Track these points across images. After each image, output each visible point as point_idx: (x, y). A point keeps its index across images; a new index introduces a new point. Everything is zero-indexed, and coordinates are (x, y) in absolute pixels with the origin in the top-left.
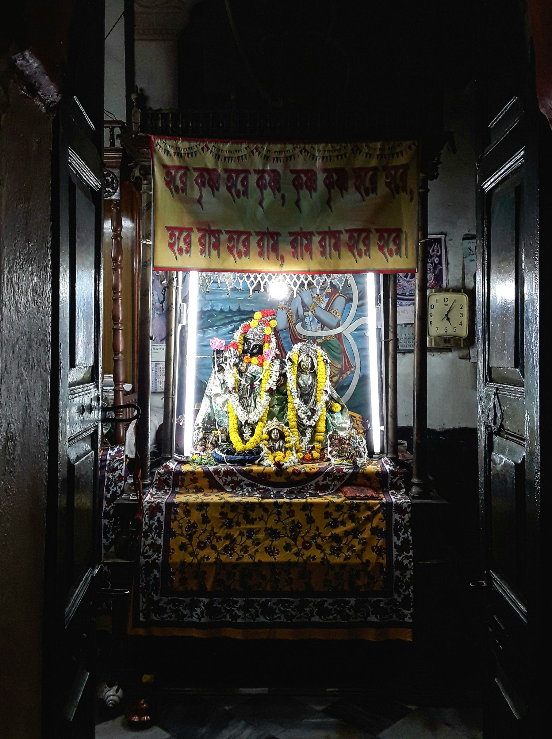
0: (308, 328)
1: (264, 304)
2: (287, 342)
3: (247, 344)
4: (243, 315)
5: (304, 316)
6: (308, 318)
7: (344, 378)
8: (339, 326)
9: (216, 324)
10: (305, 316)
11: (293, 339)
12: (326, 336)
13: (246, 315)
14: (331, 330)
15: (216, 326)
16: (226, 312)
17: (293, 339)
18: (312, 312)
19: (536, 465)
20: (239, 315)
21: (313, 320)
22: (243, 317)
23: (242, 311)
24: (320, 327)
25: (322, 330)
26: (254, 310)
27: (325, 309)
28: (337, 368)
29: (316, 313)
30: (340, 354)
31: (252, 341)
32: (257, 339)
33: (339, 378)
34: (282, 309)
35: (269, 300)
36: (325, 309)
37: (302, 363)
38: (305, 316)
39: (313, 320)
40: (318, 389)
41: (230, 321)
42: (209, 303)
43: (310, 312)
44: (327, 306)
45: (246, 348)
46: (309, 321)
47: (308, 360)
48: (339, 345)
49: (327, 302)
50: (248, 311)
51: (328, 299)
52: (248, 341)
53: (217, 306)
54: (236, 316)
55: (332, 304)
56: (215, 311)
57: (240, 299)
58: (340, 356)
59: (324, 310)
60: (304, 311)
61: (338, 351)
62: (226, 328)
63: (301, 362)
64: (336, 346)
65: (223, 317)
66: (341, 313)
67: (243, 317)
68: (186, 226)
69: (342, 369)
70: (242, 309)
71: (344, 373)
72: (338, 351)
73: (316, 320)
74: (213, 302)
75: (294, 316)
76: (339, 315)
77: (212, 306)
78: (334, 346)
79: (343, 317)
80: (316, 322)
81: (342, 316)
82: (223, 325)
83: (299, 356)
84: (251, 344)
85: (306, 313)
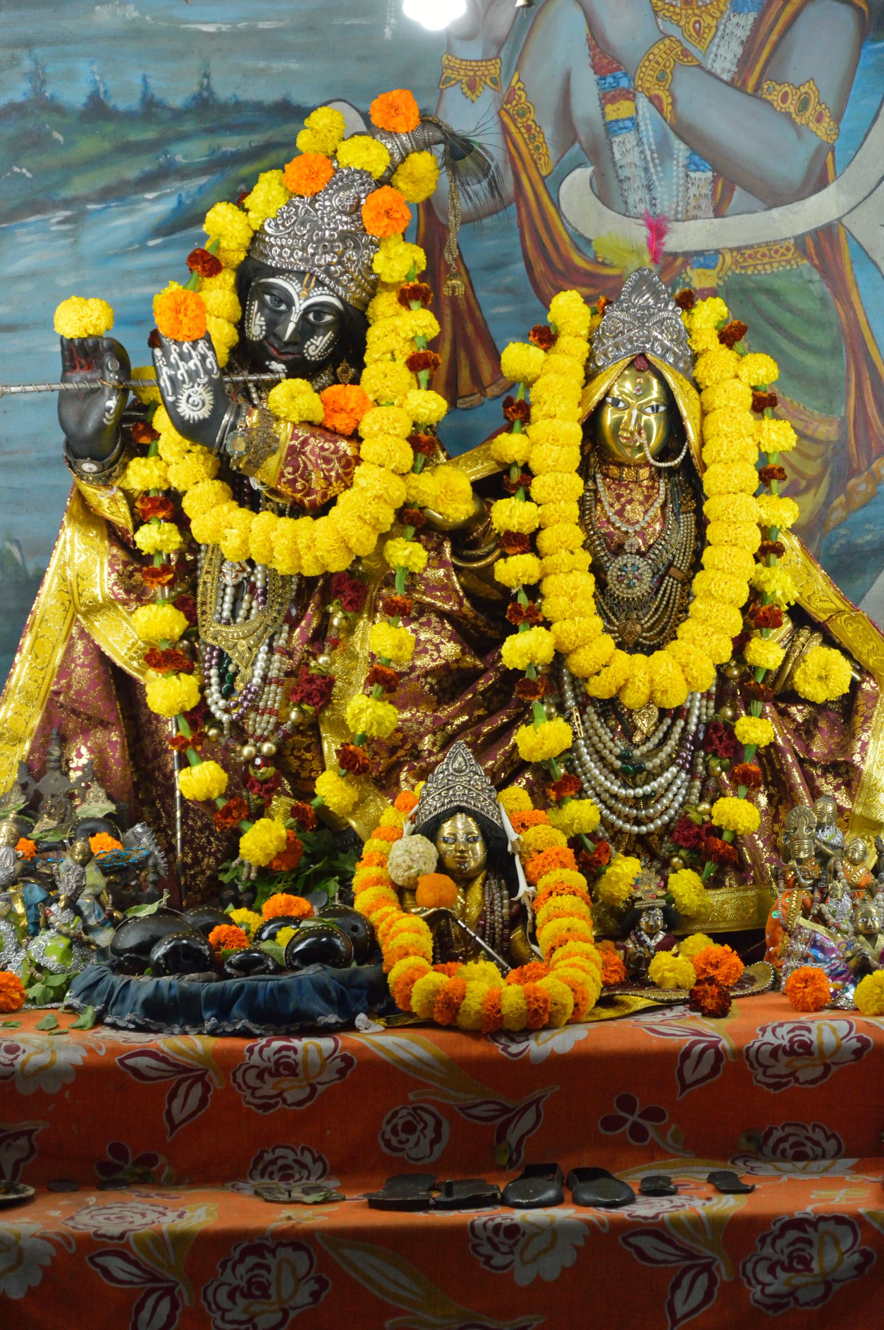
0: (632, 198)
1: (362, 59)
2: (508, 290)
3: (263, 306)
4: (232, 129)
5: (607, 126)
6: (630, 138)
7: (858, 499)
8: (822, 183)
9: (66, 193)
10: (611, 128)
11: (540, 267)
12: (738, 249)
13: (249, 127)
14: (775, 213)
15: (66, 204)
16: (128, 117)
17: (540, 267)
18: (655, 101)
19: (585, 290)
20: (210, 131)
21: (663, 151)
22: (232, 143)
23: (224, 108)
24: (706, 190)
25: (718, 213)
26: (299, 98)
27: (737, 84)
28: (817, 441)
29: (680, 107)
30: (834, 352)
31: (292, 287)
32: (327, 272)
33: (827, 504)
34: (472, 86)
35: (388, 32)
36: (737, 84)
37: (609, 417)
38: (611, 128)
39: (663, 151)
40: (275, 644)
41: (148, 168)
42: (14, 61)
43: (643, 102)
44: (745, 63)
45: (257, 328)
46: (634, 157)
47: (644, 390)
48: (823, 300)
49: (744, 34)
50: (258, 106)
51: (751, 17)
52: (269, 289)
53: (70, 76)
54: (183, 137)
55: (776, 46)
56: (55, 108)
57: (211, 28)
58: (833, 368)
59: (730, 84)
60: (608, 97)
61: (821, 339)
62: (131, 212)
63: (601, 404)
64: (809, 305)
65: (107, 146)
66: (831, 99)
67: (232, 143)
68: (680, 224)
69: (841, 445)
70: (224, 92)
71: (854, 473)
72: (821, 339)
73: (680, 149)
74: (38, 52)
75: (548, 131)
76: (819, 119)
77: (38, 78)
78: (790, 309)
79: (845, 125)
80: (682, 161)
81: (838, 119)
82: (107, 195)
83: (590, 377)
84: (290, 303)
85: (621, 110)
